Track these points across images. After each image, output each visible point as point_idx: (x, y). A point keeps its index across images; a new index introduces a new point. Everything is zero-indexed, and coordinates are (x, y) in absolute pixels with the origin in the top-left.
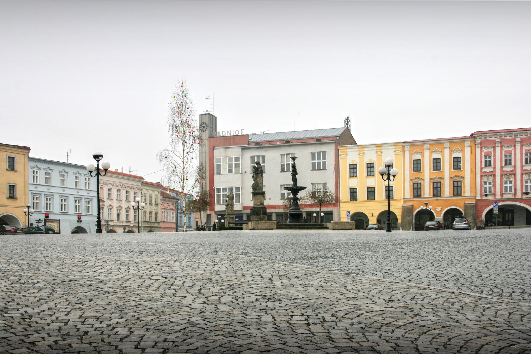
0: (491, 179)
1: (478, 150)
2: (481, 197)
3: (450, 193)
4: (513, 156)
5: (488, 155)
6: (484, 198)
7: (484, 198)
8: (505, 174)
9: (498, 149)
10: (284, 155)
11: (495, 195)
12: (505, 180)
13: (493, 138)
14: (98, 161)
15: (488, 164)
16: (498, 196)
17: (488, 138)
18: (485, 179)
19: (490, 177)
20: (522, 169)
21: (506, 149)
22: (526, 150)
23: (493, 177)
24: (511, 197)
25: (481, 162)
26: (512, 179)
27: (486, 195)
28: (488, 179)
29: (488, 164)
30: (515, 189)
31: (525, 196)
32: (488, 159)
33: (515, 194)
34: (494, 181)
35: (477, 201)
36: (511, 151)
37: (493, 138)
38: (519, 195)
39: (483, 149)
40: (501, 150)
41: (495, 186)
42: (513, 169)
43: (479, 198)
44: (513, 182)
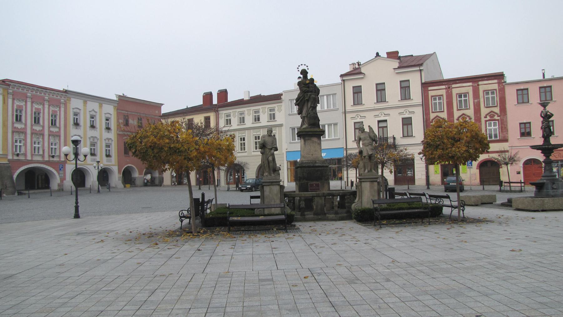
0: (22, 137)
1: (10, 101)
2: (13, 156)
3: (220, 204)
4: (58, 117)
5: (19, 109)
6: (16, 158)
7: (16, 158)
8: (17, 132)
9: (29, 104)
10: (330, 95)
11: (25, 155)
12: (34, 139)
13: (25, 91)
14: (76, 146)
15: (18, 119)
16: (29, 158)
17: (20, 90)
18: (16, 137)
19: (21, 134)
20: (50, 131)
21: (36, 107)
22: (17, 105)
23: (24, 135)
24: (39, 158)
25: (13, 115)
26: (41, 140)
27: (18, 155)
28: (19, 136)
29: (18, 119)
30: (44, 151)
31: (51, 159)
32: (19, 114)
33: (43, 156)
34: (25, 140)
35: (9, 160)
36: (22, 106)
37: (25, 91)
38: (46, 158)
39: (15, 101)
40: (32, 106)
41: (25, 145)
42: (41, 128)
43: (10, 157)
44: (41, 143)
